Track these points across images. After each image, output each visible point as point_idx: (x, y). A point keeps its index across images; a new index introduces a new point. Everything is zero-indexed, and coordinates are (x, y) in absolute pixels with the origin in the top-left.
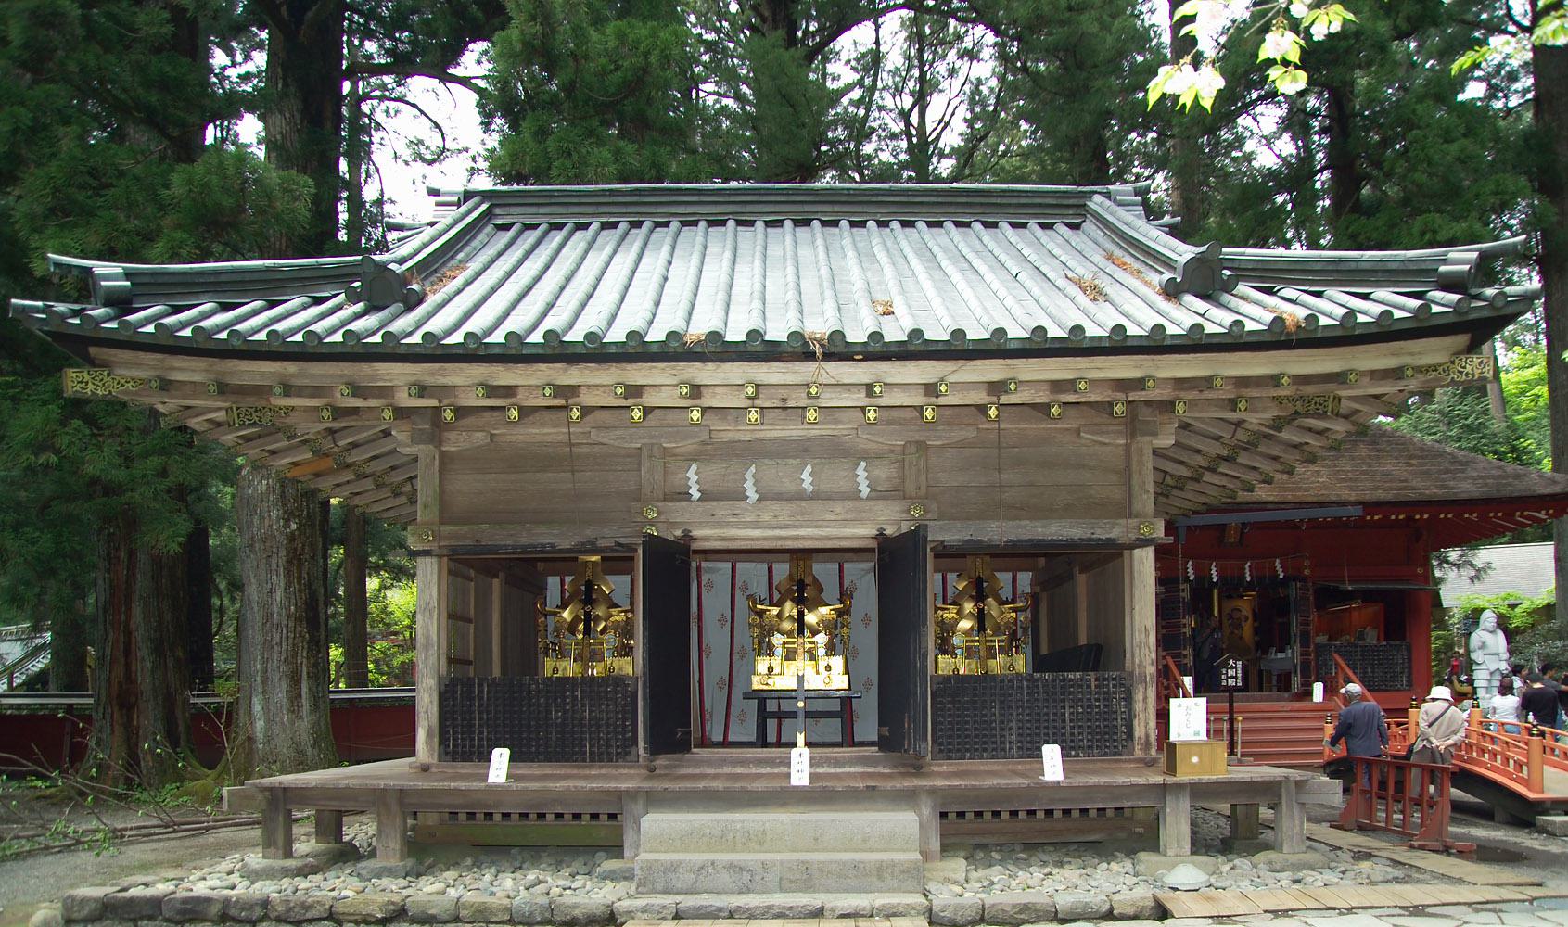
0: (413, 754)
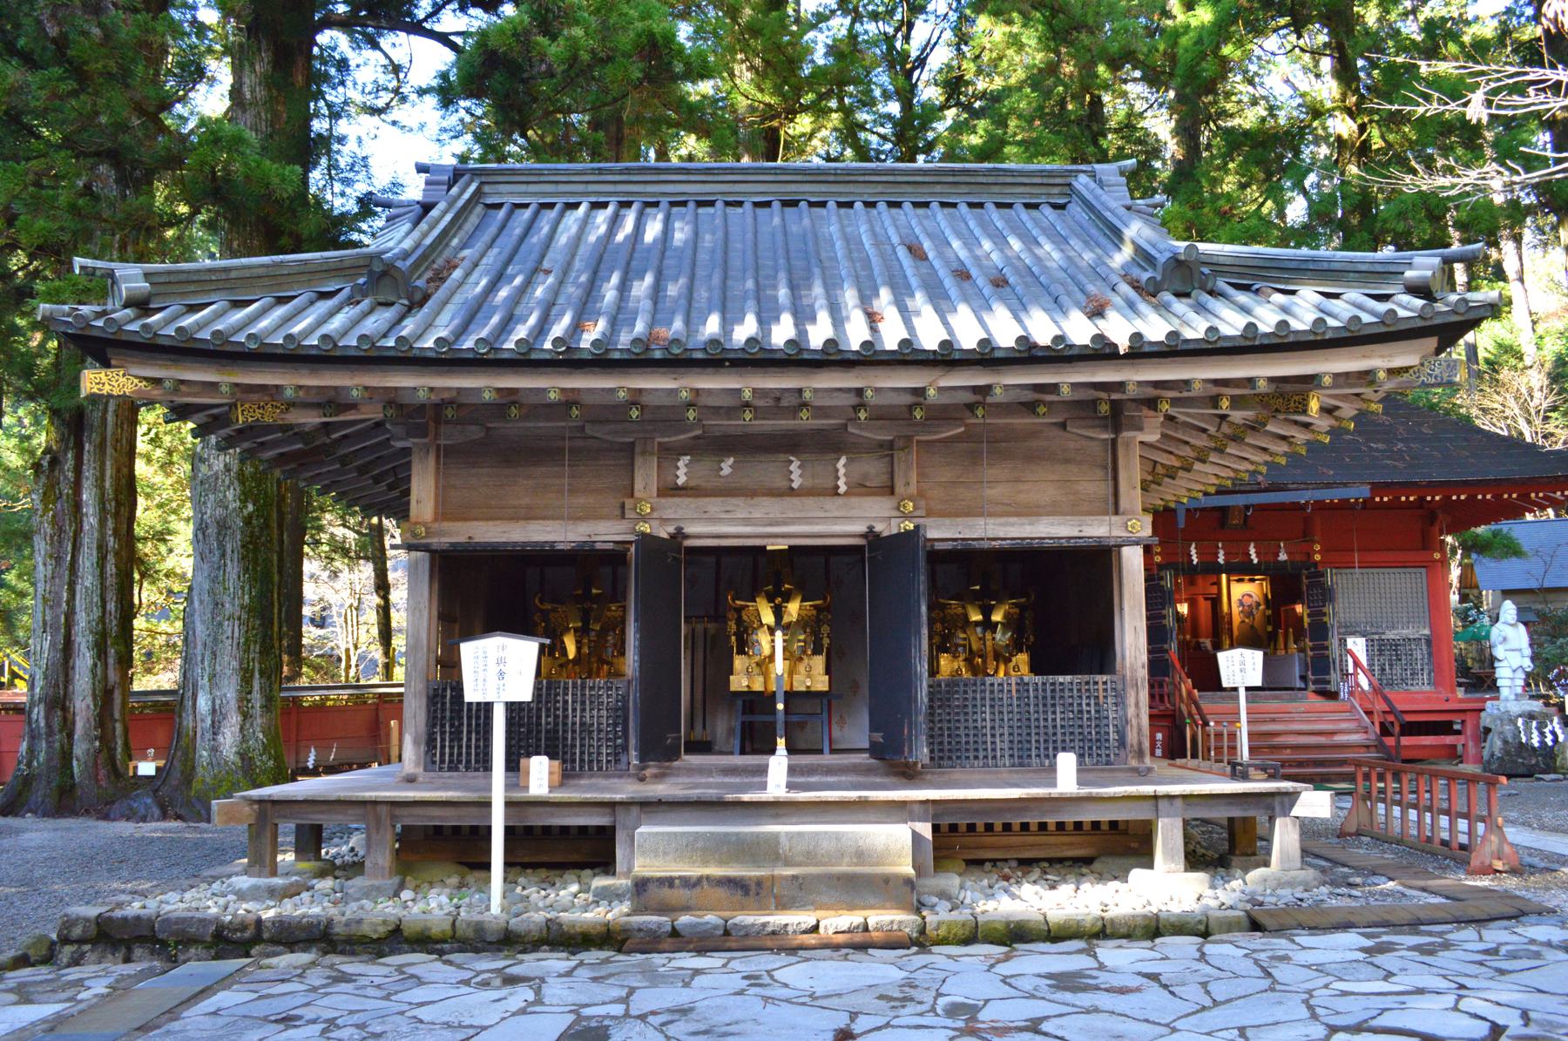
0: (1267, 864)
